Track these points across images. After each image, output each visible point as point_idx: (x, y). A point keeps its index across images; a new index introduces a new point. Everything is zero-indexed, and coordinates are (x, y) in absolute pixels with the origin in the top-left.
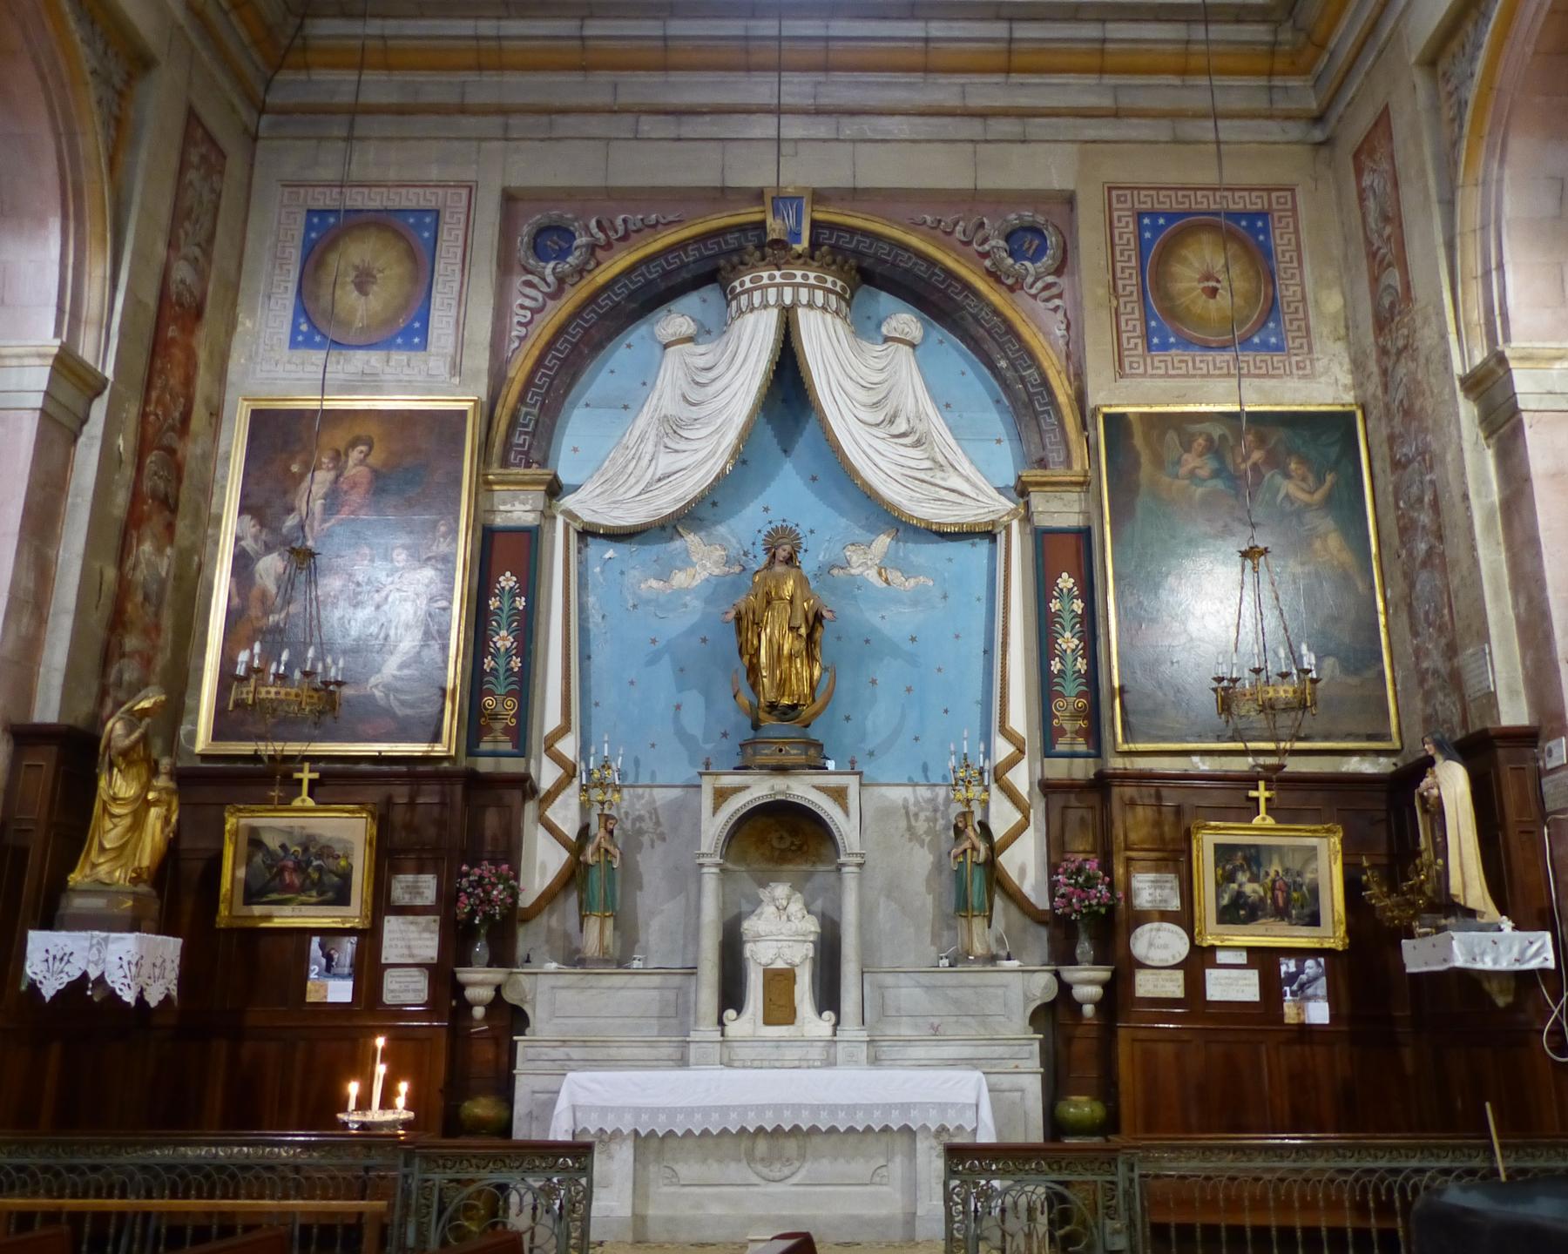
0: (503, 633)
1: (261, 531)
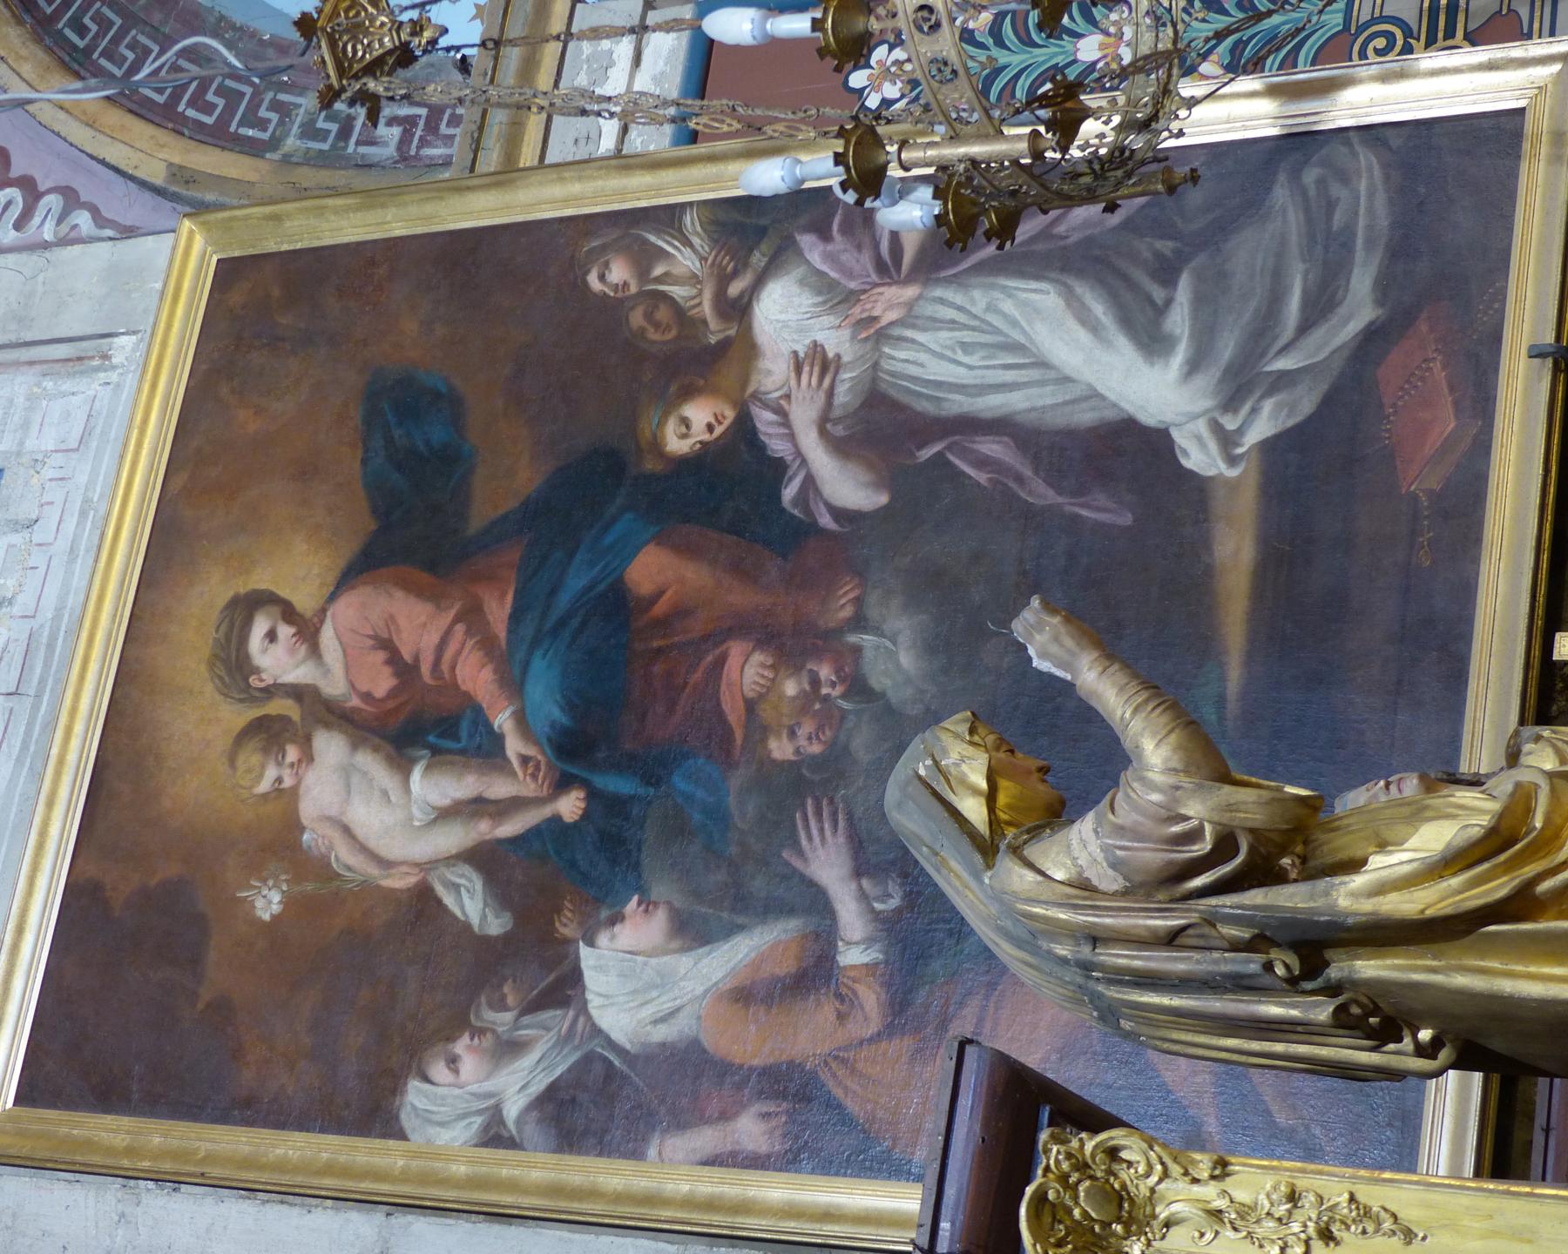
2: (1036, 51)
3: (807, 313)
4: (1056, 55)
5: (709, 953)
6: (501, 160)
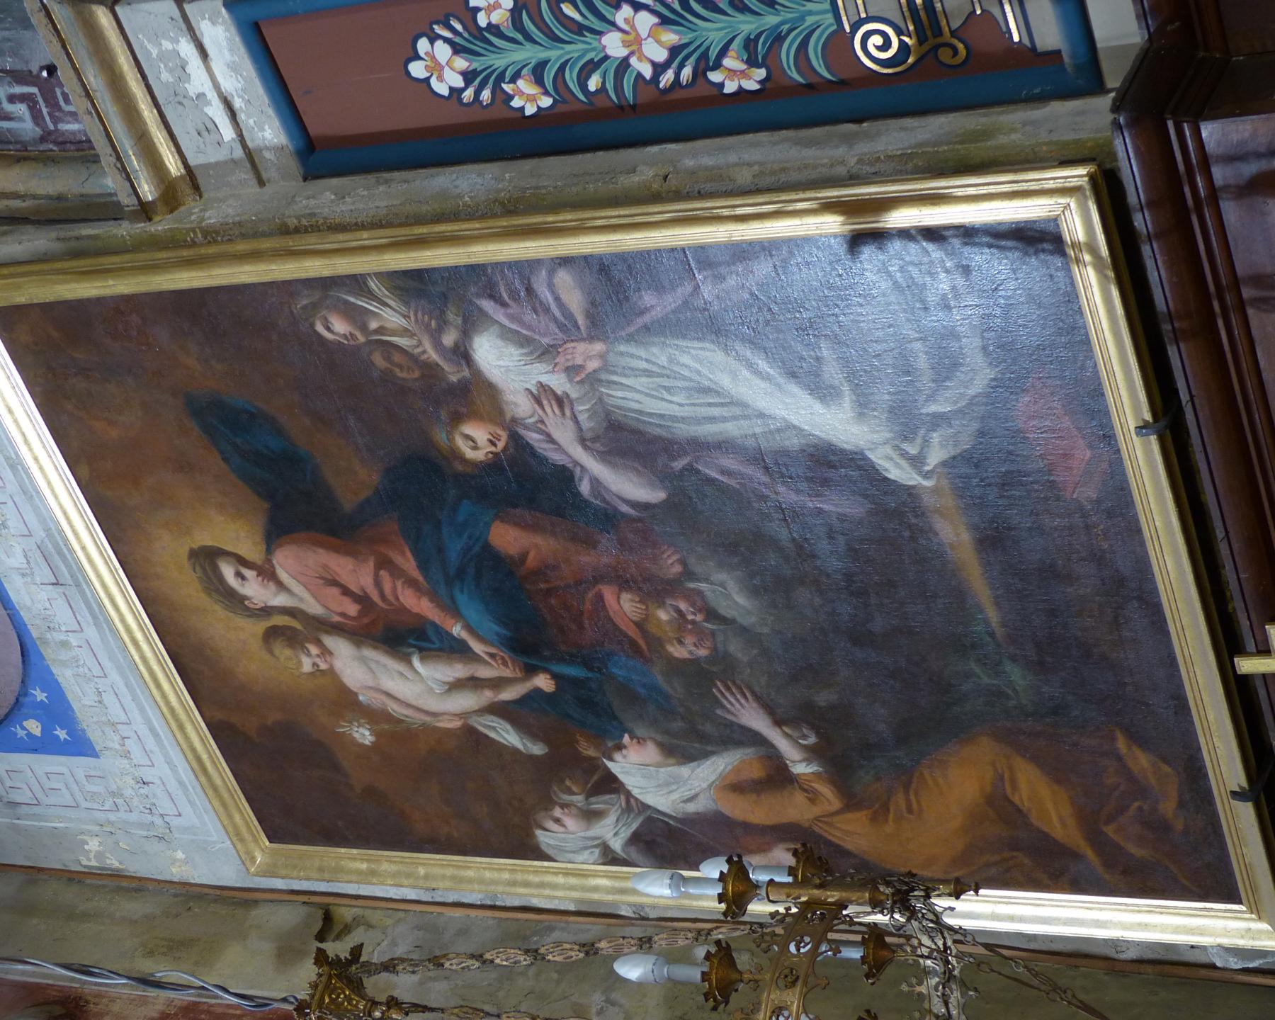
0: (613, 45)
2: (568, 47)
3: (520, 361)
4: (586, 52)
5: (699, 766)
6: (152, 174)
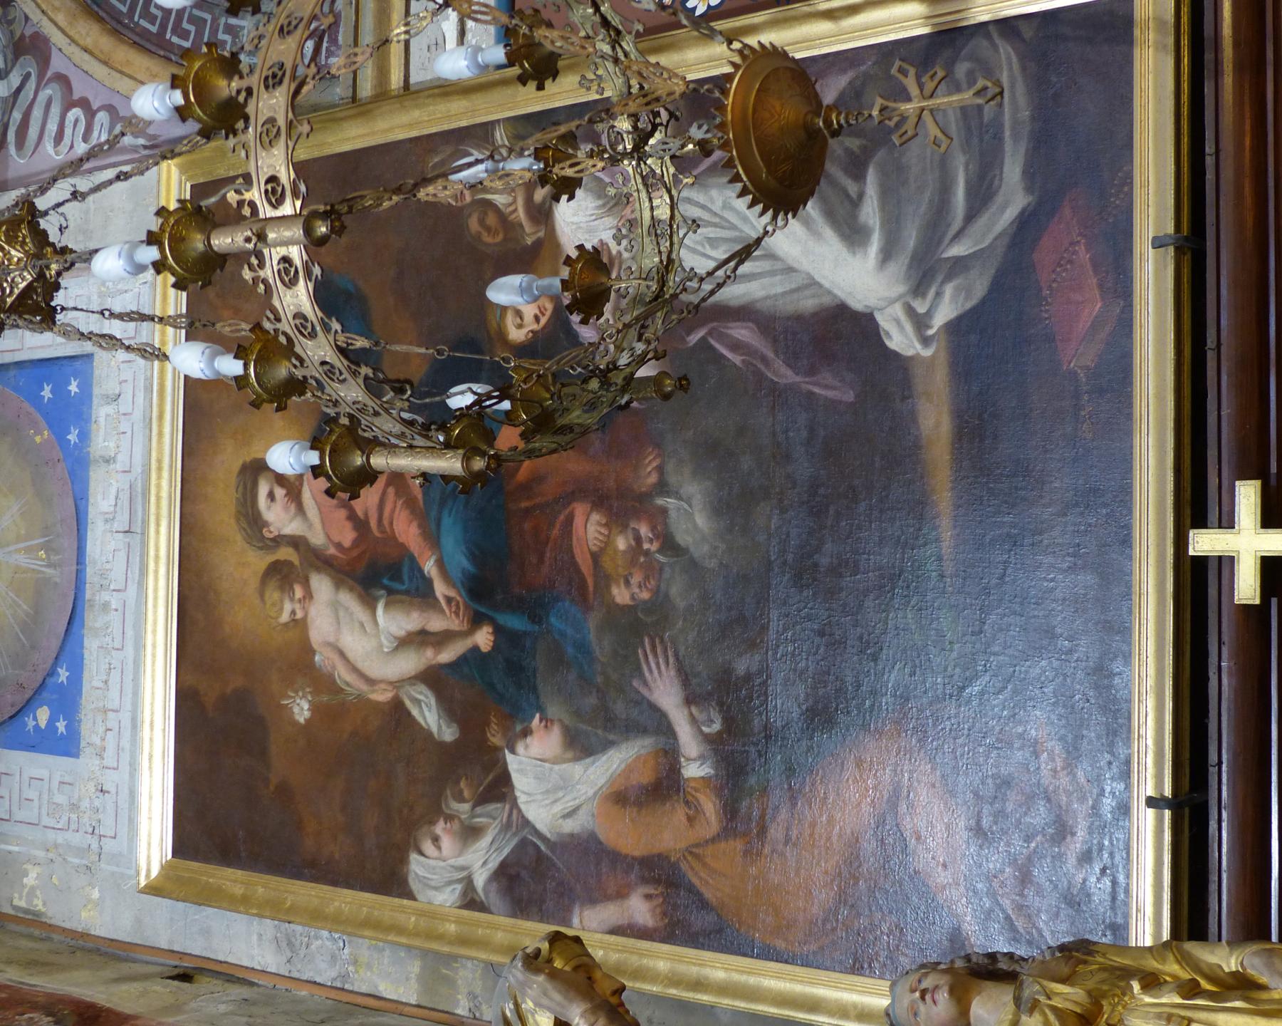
1: (449, 818)
